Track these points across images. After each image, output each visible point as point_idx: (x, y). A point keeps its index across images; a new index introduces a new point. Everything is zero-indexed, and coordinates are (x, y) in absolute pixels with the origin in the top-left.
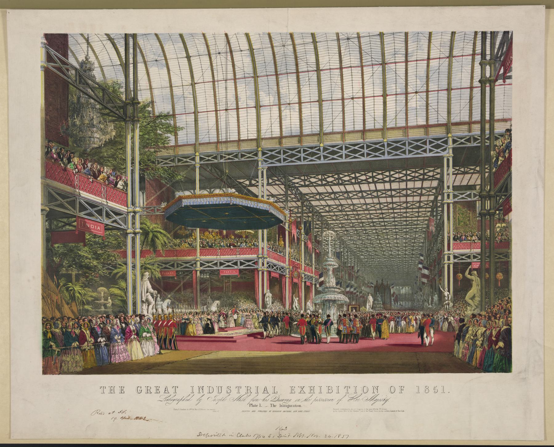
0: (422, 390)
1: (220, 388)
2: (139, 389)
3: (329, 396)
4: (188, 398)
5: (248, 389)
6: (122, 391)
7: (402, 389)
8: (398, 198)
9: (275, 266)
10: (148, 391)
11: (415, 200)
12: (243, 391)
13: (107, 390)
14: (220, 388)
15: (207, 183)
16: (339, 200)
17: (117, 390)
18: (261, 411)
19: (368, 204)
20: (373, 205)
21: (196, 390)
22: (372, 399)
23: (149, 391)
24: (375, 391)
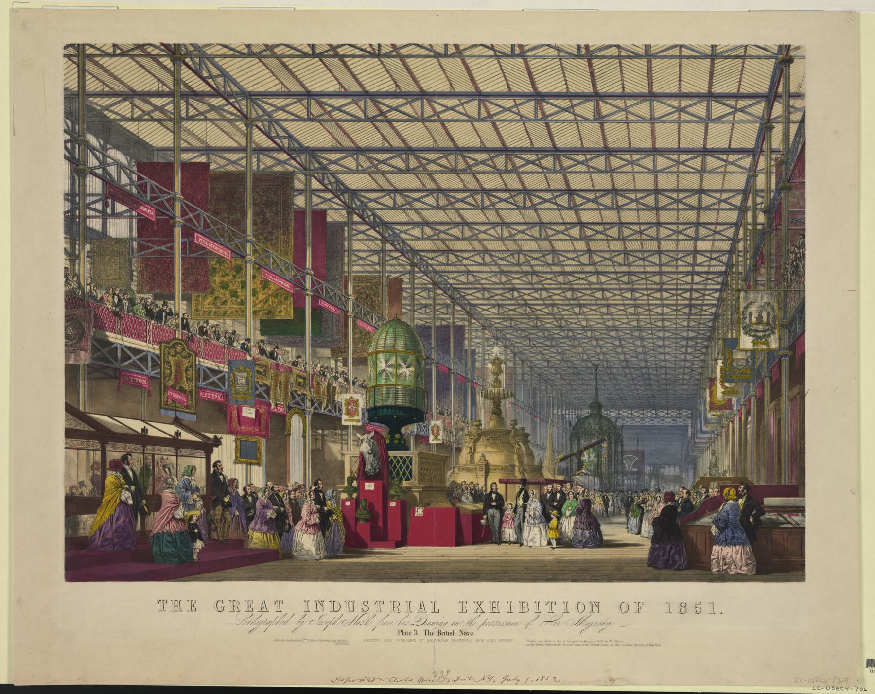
0: (675, 608)
1: (351, 603)
2: (220, 604)
3: (510, 618)
4: (285, 619)
5: (495, 607)
6: (193, 608)
7: (639, 606)
8: (639, 243)
9: (213, 384)
10: (177, 605)
11: (681, 248)
12: (559, 609)
13: (169, 606)
14: (351, 603)
15: (211, 187)
16: (515, 240)
17: (185, 606)
18: (368, 640)
19: (596, 252)
20: (607, 255)
21: (312, 606)
22: (579, 622)
23: (396, 610)
24: (320, 607)
